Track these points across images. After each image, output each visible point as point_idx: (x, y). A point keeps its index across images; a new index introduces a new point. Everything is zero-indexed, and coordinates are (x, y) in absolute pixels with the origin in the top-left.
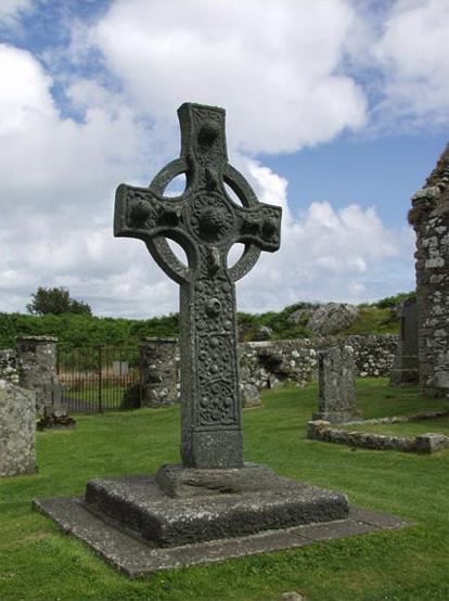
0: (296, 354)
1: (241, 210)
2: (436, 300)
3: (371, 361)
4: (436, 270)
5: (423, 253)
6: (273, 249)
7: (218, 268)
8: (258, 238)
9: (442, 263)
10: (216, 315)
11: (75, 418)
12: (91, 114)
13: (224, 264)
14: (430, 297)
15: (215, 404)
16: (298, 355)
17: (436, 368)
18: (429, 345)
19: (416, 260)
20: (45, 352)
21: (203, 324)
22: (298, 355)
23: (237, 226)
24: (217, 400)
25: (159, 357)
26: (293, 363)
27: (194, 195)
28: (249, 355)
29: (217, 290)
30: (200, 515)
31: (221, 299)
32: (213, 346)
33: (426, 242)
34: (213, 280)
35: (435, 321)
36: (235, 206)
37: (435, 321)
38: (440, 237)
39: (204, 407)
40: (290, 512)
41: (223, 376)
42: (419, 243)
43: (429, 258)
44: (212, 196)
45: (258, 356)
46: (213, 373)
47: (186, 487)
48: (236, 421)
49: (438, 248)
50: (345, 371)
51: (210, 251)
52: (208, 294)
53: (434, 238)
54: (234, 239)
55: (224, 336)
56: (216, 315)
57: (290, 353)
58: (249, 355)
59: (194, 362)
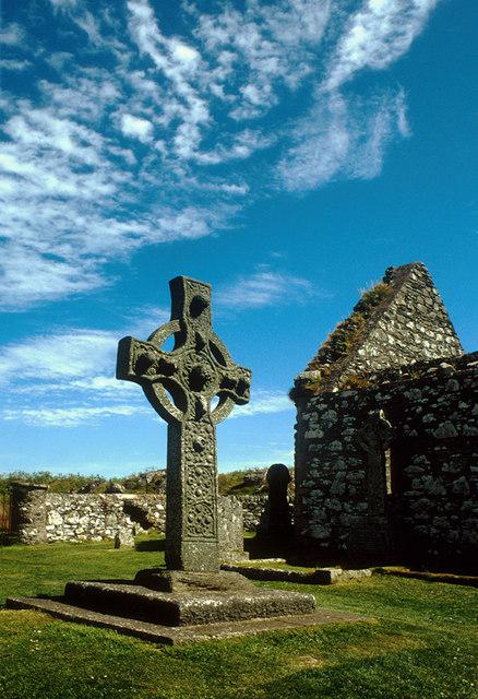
4: (316, 441)
5: (302, 426)
8: (233, 391)
9: (321, 434)
10: (202, 449)
13: (208, 408)
15: (199, 521)
17: (311, 522)
18: (304, 502)
21: (191, 456)
23: (218, 381)
24: (200, 518)
25: (30, 500)
27: (186, 353)
28: (117, 505)
30: (208, 602)
32: (198, 474)
33: (306, 417)
38: (321, 413)
39: (190, 522)
41: (206, 499)
42: (299, 417)
44: (200, 354)
45: (124, 506)
46: (198, 495)
47: (181, 584)
48: (215, 535)
49: (318, 422)
50: (234, 518)
51: (198, 399)
52: (195, 432)
55: (206, 467)
56: (202, 449)
58: (117, 505)
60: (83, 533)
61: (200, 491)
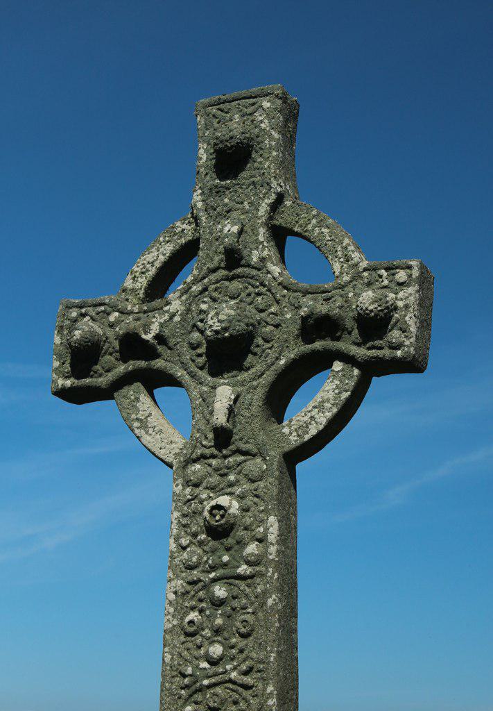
55: (242, 578)
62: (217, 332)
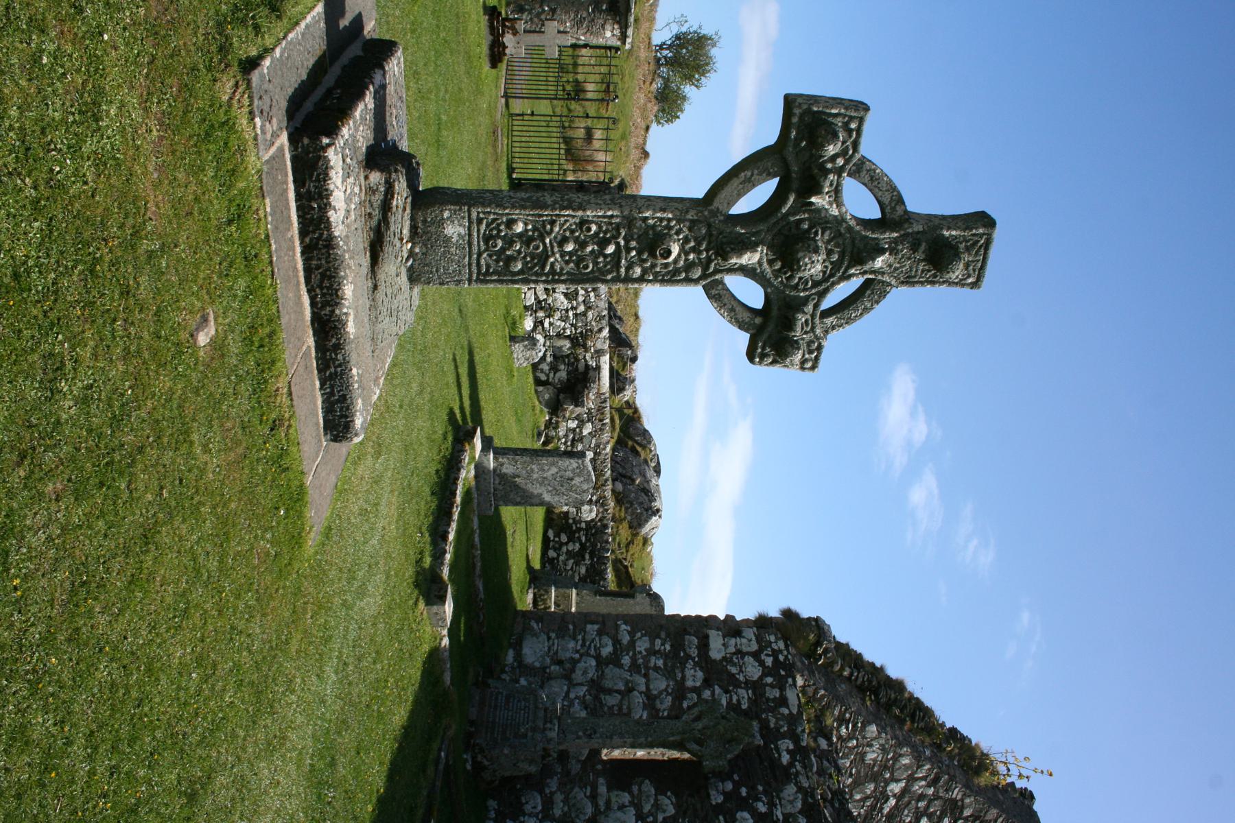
0: (588, 429)
1: (816, 306)
2: (658, 642)
3: (571, 547)
4: (704, 645)
5: (731, 627)
6: (751, 355)
7: (725, 259)
8: (771, 327)
11: (503, 66)
12: (785, 748)
13: (731, 270)
14: (663, 635)
16: (585, 432)
18: (589, 627)
19: (722, 617)
20: (608, 27)
22: (585, 432)
26: (573, 424)
29: (691, 256)
31: (676, 261)
32: (603, 243)
33: (750, 633)
34: (707, 250)
35: (626, 639)
36: (822, 295)
37: (626, 639)
40: (343, 398)
42: (746, 622)
43: (724, 637)
53: (754, 647)
54: (769, 290)
57: (589, 421)
59: (580, 213)
60: (536, 298)
61: (570, 247)
62: (798, 261)
